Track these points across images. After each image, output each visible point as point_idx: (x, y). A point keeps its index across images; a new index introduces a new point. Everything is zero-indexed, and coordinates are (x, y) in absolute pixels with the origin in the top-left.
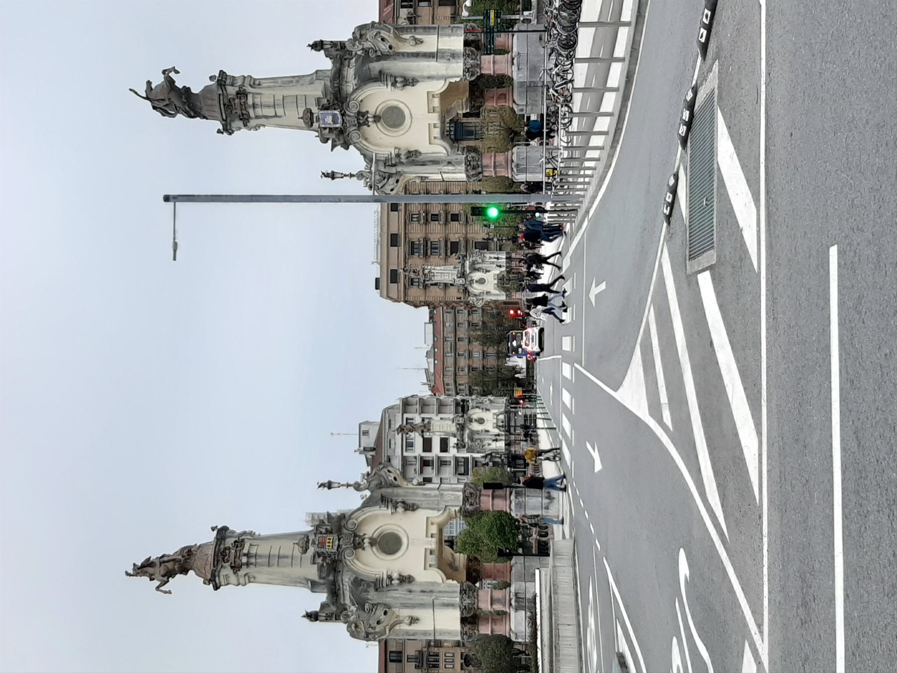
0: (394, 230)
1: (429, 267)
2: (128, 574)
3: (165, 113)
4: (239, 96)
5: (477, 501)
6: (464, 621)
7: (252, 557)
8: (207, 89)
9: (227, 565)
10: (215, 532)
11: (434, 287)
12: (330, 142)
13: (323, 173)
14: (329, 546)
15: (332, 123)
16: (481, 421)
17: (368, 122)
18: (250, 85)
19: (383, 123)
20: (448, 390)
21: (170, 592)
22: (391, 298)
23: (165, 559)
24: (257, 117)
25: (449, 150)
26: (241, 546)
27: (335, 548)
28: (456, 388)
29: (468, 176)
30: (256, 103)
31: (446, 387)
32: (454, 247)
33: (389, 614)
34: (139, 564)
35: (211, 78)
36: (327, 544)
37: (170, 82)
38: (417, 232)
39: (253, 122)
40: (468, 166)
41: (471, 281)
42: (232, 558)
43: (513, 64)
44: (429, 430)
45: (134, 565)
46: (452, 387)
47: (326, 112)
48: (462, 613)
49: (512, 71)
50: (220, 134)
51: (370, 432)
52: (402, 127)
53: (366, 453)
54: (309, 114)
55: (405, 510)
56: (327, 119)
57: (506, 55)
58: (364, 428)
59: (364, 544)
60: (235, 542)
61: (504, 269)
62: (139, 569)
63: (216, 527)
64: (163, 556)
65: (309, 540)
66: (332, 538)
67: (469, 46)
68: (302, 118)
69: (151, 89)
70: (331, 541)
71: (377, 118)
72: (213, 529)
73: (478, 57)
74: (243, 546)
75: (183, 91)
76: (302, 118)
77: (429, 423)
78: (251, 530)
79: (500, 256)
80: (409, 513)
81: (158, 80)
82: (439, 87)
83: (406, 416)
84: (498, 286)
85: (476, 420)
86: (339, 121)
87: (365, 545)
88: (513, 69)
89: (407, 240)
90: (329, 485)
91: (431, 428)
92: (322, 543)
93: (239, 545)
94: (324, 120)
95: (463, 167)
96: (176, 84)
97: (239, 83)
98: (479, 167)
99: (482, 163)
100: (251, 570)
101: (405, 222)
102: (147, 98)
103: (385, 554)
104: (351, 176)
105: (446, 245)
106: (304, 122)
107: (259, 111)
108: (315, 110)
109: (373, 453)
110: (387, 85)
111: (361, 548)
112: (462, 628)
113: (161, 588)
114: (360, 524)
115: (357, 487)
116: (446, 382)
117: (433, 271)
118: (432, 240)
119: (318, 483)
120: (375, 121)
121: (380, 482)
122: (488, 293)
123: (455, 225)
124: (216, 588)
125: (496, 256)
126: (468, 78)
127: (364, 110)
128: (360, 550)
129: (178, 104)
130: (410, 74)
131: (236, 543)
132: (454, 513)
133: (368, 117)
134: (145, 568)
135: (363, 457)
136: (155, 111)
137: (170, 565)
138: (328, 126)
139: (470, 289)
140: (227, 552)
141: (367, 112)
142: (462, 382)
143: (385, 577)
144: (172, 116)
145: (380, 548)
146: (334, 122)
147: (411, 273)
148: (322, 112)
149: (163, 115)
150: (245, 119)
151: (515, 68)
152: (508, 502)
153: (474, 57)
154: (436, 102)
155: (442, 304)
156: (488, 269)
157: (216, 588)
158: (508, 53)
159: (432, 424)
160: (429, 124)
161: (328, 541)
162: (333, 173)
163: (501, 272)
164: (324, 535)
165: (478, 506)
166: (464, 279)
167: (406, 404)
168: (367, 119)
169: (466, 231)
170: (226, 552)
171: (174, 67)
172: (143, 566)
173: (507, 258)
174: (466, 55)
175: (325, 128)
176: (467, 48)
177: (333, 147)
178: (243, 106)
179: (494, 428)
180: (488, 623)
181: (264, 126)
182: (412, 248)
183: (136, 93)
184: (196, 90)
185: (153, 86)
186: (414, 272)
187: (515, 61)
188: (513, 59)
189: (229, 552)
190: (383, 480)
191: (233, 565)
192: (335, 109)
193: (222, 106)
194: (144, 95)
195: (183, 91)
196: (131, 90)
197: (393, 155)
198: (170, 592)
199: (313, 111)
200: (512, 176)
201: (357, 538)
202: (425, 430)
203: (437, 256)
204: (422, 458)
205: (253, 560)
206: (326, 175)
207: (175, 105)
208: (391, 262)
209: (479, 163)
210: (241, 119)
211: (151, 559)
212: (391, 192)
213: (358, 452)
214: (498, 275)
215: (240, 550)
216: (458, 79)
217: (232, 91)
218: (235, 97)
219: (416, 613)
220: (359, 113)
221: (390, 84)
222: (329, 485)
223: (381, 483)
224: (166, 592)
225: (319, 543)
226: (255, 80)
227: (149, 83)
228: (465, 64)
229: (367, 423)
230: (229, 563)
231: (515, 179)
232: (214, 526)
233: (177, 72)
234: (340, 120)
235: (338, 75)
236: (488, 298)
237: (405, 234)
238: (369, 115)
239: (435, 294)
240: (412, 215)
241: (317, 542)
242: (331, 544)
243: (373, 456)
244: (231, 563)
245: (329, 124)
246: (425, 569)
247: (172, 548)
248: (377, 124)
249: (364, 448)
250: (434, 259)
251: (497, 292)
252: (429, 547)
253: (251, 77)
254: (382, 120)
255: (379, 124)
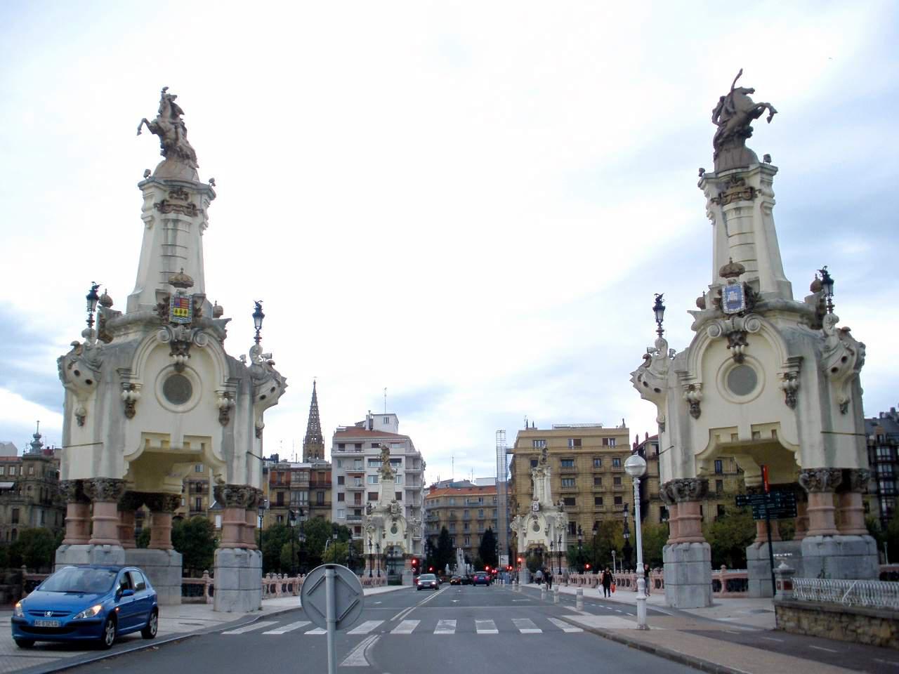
0: (584, 443)
1: (549, 474)
2: (165, 89)
3: (717, 113)
4: (749, 190)
5: (233, 504)
6: (79, 483)
7: (174, 226)
8: (751, 155)
9: (167, 197)
10: (208, 183)
11: (530, 483)
12: (699, 309)
13: (661, 296)
14: (176, 312)
15: (728, 300)
16: (394, 530)
17: (734, 347)
18: (763, 203)
19: (733, 367)
20: (433, 502)
21: (139, 133)
22: (517, 442)
23: (180, 130)
24: (724, 214)
25: (703, 457)
26: (188, 212)
27: (174, 320)
28: (435, 509)
29: (668, 484)
30: (742, 212)
31: (435, 500)
32: (570, 502)
33: (86, 386)
34: (175, 102)
35: (768, 158)
36: (179, 309)
37: (755, 112)
38: (583, 464)
39: (717, 209)
40: (683, 483)
41: (535, 517)
42: (173, 202)
43: (825, 536)
44: (384, 478)
45: (175, 97)
46: (436, 505)
47: (742, 291)
48: (87, 481)
49: (814, 536)
50: (698, 173)
51: (386, 426)
52: (730, 392)
53: (368, 422)
54: (737, 270)
55: (221, 409)
56: (734, 296)
57: (835, 527)
58: (391, 419)
59: (177, 355)
60: (194, 206)
61: (549, 550)
62: (169, 100)
63: (214, 185)
64: (185, 130)
65: (186, 288)
66: (187, 315)
67: (843, 475)
68: (731, 262)
69: (746, 94)
70: (183, 315)
71: (739, 358)
72: (212, 181)
73: (830, 488)
74: (189, 214)
75: (746, 127)
76: (731, 262)
77: (392, 478)
78: (209, 226)
79: (562, 544)
80: (217, 415)
81: (756, 99)
82: (787, 437)
83: (404, 459)
84: (531, 545)
85: (395, 524)
86: (732, 310)
87: (175, 356)
88: (818, 537)
89: (576, 455)
90: (259, 315)
91: (387, 480)
92: (181, 303)
93: (189, 210)
94: (731, 290)
95: (679, 476)
96: (754, 120)
97: (765, 190)
98: (682, 497)
99: (685, 501)
100: (157, 225)
101: (592, 453)
102: (733, 90)
103: (163, 382)
104: (660, 332)
105: (570, 494)
106: (727, 266)
107: (731, 216)
108: (742, 279)
109: (367, 429)
110: (783, 367)
111: (173, 352)
112: (71, 482)
113: (144, 124)
114: (201, 349)
115: (255, 351)
116: (440, 499)
117: (545, 478)
118: (576, 479)
119: (826, 267)
120: (735, 355)
121: (259, 377)
122: (525, 535)
123: (591, 501)
124: (141, 186)
125: (562, 541)
126: (801, 476)
127: (749, 340)
128: (169, 351)
129: (730, 125)
130: (802, 398)
131: (192, 207)
132: (218, 473)
133: (740, 346)
134: (170, 107)
135: (364, 419)
136: (718, 100)
137: (171, 135)
138: (724, 295)
139: (528, 516)
140: (183, 197)
141: (747, 345)
142: (440, 514)
143: (132, 381)
144: (715, 120)
145: (172, 376)
146: (730, 304)
147: (543, 457)
148: (741, 287)
149: (714, 111)
150: (720, 200)
151: (819, 539)
152: (232, 545)
153: (830, 482)
154: (766, 435)
155: (514, 492)
156: (549, 534)
157: (141, 186)
158: (838, 529)
159: (390, 480)
160: (736, 427)
161: (183, 310)
162: (663, 309)
163: (547, 547)
164: (190, 306)
165: (227, 505)
166: (538, 509)
167: (416, 459)
168: (737, 344)
169: (586, 513)
170: (181, 195)
171: (776, 112)
172: (174, 106)
173: (561, 552)
174: (832, 471)
175: (720, 293)
176: (840, 473)
177: (694, 313)
178: (736, 196)
179: (388, 543)
180: (78, 516)
181: (714, 224)
182: (567, 460)
183: (738, 77)
184: (749, 143)
185: (749, 95)
186: (544, 459)
187: (828, 539)
188: (831, 536)
189: (182, 199)
190: (261, 382)
191: (165, 203)
192: (746, 303)
193: (734, 171)
194: (735, 87)
195: (746, 127)
196: (741, 71)
197: (692, 382)
198: (139, 133)
199: (741, 276)
200: (670, 545)
201: (184, 347)
202: (384, 475)
203: (560, 485)
204: (363, 474)
205: (170, 226)
206: (659, 301)
207: (728, 120)
208: (555, 440)
209: (687, 498)
210: (720, 195)
211: (181, 116)
212: (642, 383)
213: (368, 414)
214: (543, 544)
215: (183, 211)
216: (799, 463)
217: (755, 182)
218: (746, 186)
219: (90, 422)
220: (745, 333)
221: (787, 370)
222: (259, 315)
223: (259, 379)
224: (139, 129)
225: (181, 299)
226: (771, 209)
227: (752, 91)
228: (821, 470)
229: (397, 422)
230: (168, 199)
231: (666, 549)
232: (215, 183)
233: (769, 120)
234: (732, 311)
235: (790, 310)
236: (519, 535)
237: (581, 453)
238: (743, 346)
239: (523, 485)
240: (600, 459)
241: (182, 297)
242: (178, 314)
243: (365, 428)
244: (167, 201)
245: (727, 297)
246: (143, 433)
247: (195, 138)
248: (732, 357)
249: (372, 420)
250: (558, 482)
251: (526, 544)
252: (172, 439)
253: (774, 204)
254: (738, 365)
255: (732, 360)
